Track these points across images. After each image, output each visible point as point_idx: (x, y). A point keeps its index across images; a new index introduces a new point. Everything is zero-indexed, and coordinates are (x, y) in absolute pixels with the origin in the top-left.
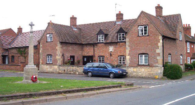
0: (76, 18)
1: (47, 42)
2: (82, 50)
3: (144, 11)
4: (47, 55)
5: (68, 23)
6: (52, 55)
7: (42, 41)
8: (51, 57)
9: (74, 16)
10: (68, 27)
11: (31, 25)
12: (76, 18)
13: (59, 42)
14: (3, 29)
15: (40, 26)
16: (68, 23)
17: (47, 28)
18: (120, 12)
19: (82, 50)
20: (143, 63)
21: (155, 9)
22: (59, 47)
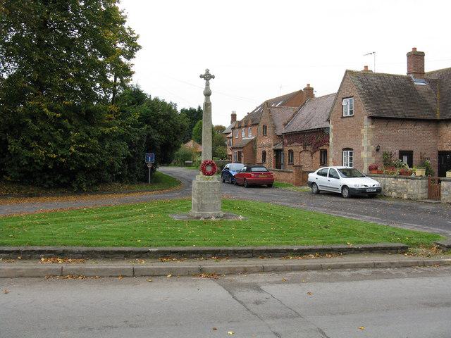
0: (422, 55)
1: (343, 117)
2: (437, 135)
3: (426, 57)
4: (344, 149)
5: (400, 68)
6: (352, 149)
7: (332, 116)
8: (351, 154)
9: (369, 69)
10: (402, 77)
11: (234, 116)
12: (422, 55)
13: (366, 118)
14: (161, 99)
15: (327, 84)
16: (400, 68)
17: (339, 90)
18: (366, 67)
19: (437, 135)
20: (349, 115)
21: (406, 57)
22: (367, 126)
